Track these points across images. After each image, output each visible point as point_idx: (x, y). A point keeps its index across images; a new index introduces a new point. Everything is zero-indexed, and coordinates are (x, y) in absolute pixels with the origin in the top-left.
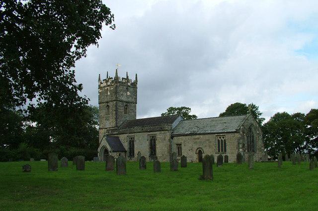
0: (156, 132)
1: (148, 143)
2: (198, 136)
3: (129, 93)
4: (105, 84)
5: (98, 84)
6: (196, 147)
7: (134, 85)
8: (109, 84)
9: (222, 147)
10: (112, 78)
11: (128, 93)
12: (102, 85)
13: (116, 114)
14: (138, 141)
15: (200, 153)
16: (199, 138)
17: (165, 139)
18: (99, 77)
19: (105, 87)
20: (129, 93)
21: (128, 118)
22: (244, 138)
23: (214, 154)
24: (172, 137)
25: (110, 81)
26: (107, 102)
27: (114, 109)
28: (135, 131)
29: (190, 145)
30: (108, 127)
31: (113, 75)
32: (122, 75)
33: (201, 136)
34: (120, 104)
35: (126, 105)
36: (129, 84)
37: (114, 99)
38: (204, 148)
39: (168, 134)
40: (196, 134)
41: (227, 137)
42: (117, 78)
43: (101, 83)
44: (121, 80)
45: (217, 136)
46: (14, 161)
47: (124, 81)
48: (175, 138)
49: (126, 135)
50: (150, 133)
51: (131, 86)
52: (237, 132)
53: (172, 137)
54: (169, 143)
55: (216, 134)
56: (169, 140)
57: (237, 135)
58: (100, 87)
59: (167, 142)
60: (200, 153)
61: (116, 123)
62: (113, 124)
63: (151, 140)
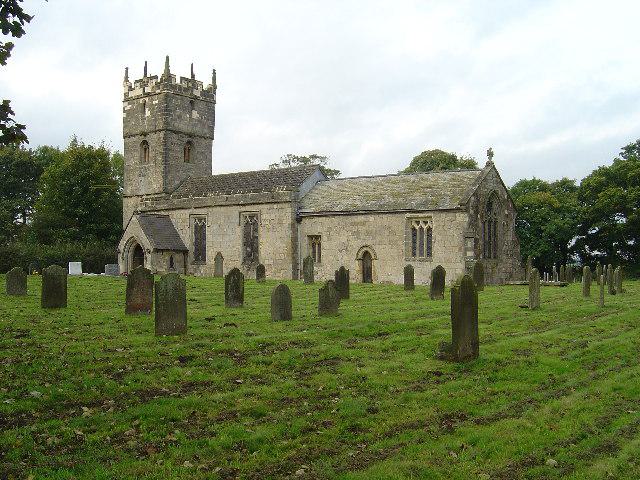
1: (239, 231)
2: (361, 218)
3: (195, 114)
4: (139, 92)
5: (122, 90)
6: (356, 244)
7: (210, 95)
9: (422, 244)
10: (156, 77)
12: (132, 94)
16: (364, 224)
17: (280, 223)
18: (127, 72)
20: (195, 114)
24: (299, 219)
27: (161, 149)
29: (344, 239)
31: (157, 70)
33: (371, 218)
35: (189, 142)
36: (197, 93)
38: (377, 249)
42: (168, 76)
44: (178, 81)
47: (184, 85)
48: (306, 221)
49: (187, 212)
50: (243, 209)
53: (299, 219)
55: (408, 215)
56: (293, 225)
58: (127, 99)
61: (165, 184)
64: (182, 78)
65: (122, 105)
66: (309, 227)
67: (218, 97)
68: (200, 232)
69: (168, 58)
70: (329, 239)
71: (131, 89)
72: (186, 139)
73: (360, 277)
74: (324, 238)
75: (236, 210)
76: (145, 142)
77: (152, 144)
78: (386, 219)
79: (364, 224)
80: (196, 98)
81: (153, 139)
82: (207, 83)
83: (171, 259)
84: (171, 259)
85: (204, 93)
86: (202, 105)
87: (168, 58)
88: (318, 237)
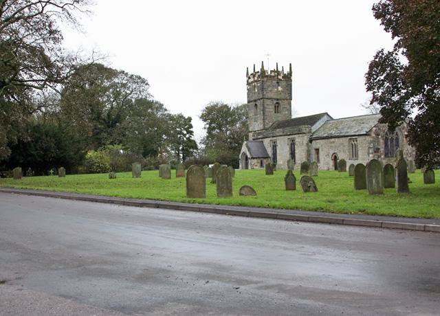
0: (296, 136)
2: (333, 140)
3: (280, 88)
4: (252, 80)
5: (246, 79)
6: (332, 152)
7: (288, 77)
8: (256, 79)
10: (258, 72)
11: (279, 87)
12: (250, 81)
13: (264, 114)
14: (279, 146)
15: (335, 158)
16: (334, 142)
17: (303, 143)
19: (252, 82)
20: (280, 88)
21: (281, 117)
22: (379, 141)
23: (347, 160)
24: (311, 141)
25: (257, 76)
26: (255, 101)
27: (262, 108)
28: (278, 134)
30: (256, 129)
31: (258, 69)
32: (269, 68)
33: (336, 140)
34: (268, 102)
35: (277, 103)
36: (280, 77)
37: (261, 97)
39: (306, 138)
40: (331, 137)
41: (360, 139)
42: (263, 71)
43: (249, 78)
44: (269, 73)
45: (350, 139)
46: (35, 175)
47: (273, 74)
48: (314, 142)
49: (270, 139)
50: (289, 137)
51: (283, 80)
52: (367, 134)
53: (311, 141)
54: (306, 148)
56: (307, 144)
57: (368, 138)
58: (248, 84)
59: (304, 148)
60: (335, 158)
61: (264, 125)
62: (261, 127)
63: (291, 144)
64: (271, 71)
65: (246, 86)
66: (316, 144)
67: (293, 78)
68: (274, 148)
69: (290, 65)
70: (322, 150)
71: (249, 78)
72: (275, 102)
73: (334, 168)
74: (320, 150)
75: (286, 137)
76: (256, 105)
77: (259, 105)
78: (341, 140)
79: (334, 142)
80: (280, 80)
81: (258, 103)
82: (286, 71)
83: (261, 162)
84: (261, 162)
85: (285, 76)
86: (284, 83)
87: (290, 65)
88: (287, 189)
